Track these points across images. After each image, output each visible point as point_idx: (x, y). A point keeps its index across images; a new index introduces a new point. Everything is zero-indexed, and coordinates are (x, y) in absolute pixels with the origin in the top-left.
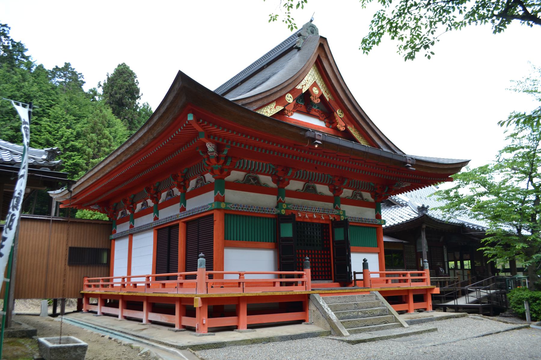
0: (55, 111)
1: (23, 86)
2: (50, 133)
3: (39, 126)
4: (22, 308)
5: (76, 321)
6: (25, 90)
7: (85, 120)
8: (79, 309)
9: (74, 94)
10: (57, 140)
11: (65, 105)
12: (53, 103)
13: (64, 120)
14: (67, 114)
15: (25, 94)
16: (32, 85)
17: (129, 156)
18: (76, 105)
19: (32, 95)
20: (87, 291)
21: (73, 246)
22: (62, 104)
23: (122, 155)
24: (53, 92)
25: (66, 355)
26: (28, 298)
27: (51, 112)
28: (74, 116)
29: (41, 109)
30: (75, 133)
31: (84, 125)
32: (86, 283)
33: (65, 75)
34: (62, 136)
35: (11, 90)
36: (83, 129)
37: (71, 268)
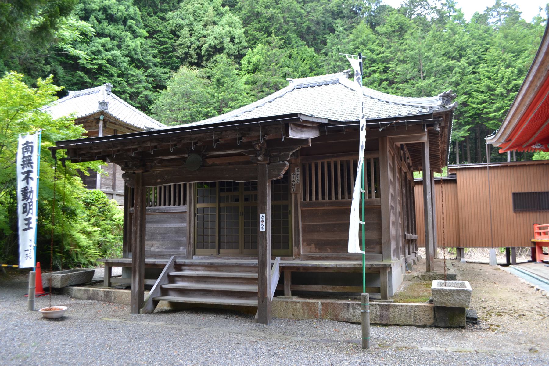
0: (491, 54)
1: (454, 40)
2: (490, 78)
3: (477, 74)
4: (480, 257)
5: (523, 271)
6: (457, 43)
7: (526, 54)
8: (534, 259)
9: (509, 29)
10: (498, 84)
11: (500, 44)
12: (488, 46)
13: (502, 61)
14: (503, 53)
15: (458, 47)
16: (463, 36)
17: (542, 78)
18: (512, 40)
19: (464, 46)
20: (538, 239)
21: (517, 192)
22: (497, 44)
23: (536, 80)
24: (486, 35)
25: (449, 298)
26: (486, 247)
27: (487, 57)
28: (513, 53)
29: (477, 57)
30: (516, 71)
31: (525, 60)
32: (537, 231)
33: (498, 13)
34: (503, 78)
35: (444, 47)
36: (525, 64)
37: (518, 215)
